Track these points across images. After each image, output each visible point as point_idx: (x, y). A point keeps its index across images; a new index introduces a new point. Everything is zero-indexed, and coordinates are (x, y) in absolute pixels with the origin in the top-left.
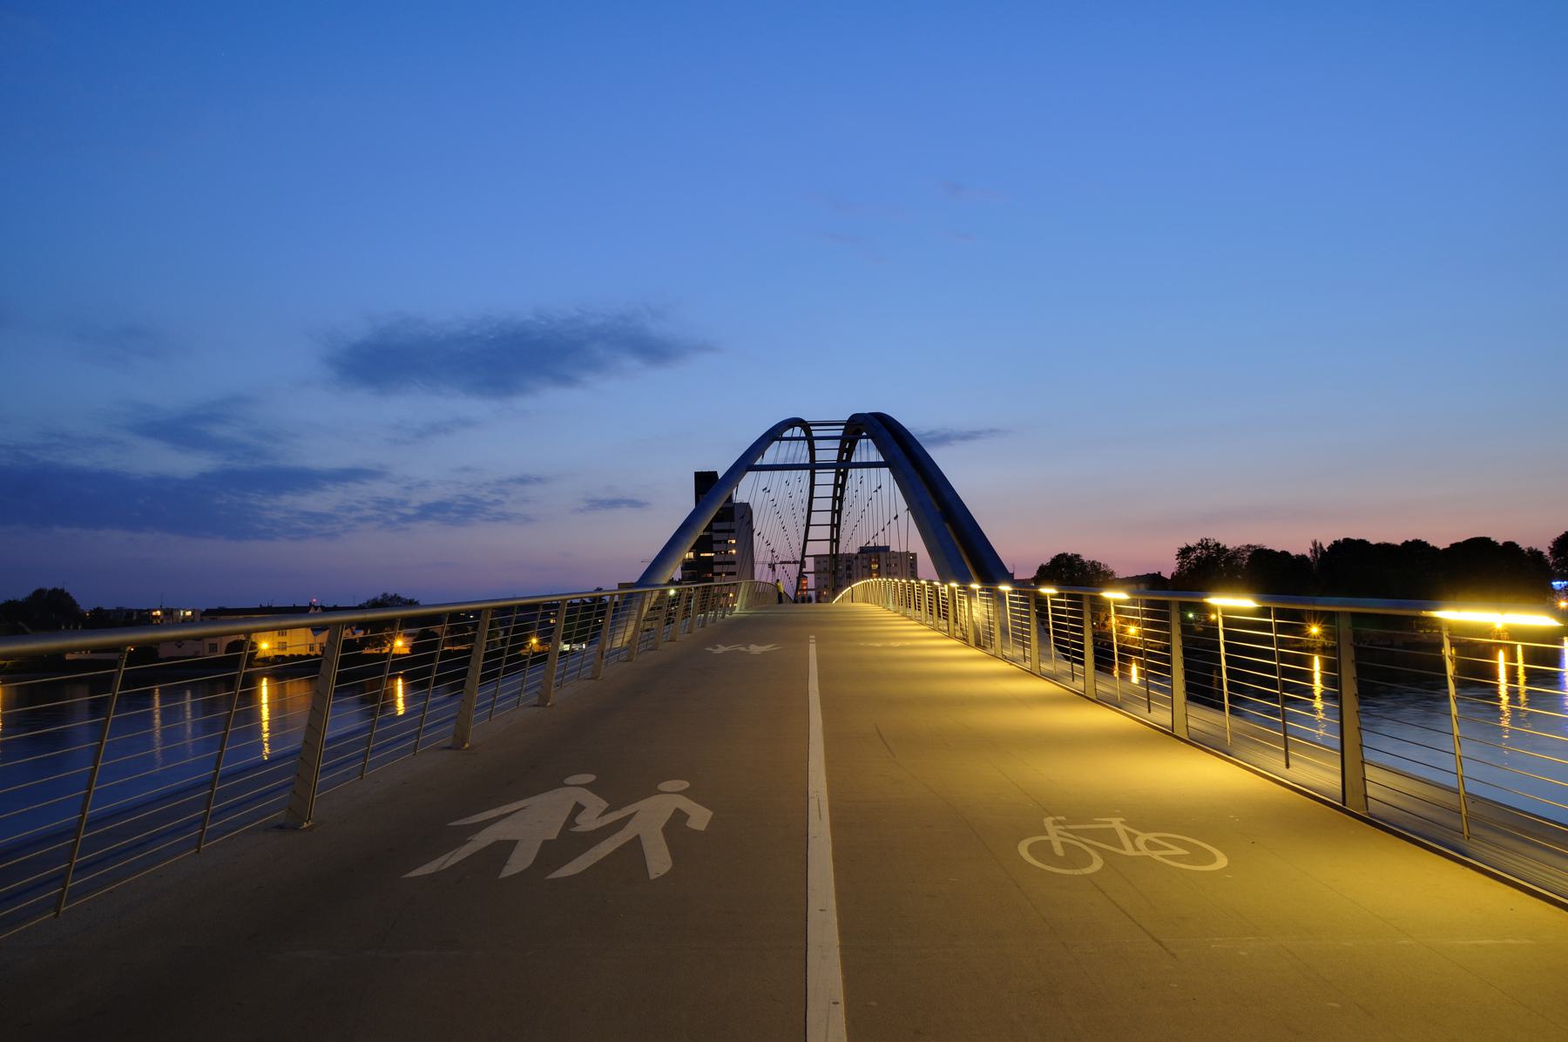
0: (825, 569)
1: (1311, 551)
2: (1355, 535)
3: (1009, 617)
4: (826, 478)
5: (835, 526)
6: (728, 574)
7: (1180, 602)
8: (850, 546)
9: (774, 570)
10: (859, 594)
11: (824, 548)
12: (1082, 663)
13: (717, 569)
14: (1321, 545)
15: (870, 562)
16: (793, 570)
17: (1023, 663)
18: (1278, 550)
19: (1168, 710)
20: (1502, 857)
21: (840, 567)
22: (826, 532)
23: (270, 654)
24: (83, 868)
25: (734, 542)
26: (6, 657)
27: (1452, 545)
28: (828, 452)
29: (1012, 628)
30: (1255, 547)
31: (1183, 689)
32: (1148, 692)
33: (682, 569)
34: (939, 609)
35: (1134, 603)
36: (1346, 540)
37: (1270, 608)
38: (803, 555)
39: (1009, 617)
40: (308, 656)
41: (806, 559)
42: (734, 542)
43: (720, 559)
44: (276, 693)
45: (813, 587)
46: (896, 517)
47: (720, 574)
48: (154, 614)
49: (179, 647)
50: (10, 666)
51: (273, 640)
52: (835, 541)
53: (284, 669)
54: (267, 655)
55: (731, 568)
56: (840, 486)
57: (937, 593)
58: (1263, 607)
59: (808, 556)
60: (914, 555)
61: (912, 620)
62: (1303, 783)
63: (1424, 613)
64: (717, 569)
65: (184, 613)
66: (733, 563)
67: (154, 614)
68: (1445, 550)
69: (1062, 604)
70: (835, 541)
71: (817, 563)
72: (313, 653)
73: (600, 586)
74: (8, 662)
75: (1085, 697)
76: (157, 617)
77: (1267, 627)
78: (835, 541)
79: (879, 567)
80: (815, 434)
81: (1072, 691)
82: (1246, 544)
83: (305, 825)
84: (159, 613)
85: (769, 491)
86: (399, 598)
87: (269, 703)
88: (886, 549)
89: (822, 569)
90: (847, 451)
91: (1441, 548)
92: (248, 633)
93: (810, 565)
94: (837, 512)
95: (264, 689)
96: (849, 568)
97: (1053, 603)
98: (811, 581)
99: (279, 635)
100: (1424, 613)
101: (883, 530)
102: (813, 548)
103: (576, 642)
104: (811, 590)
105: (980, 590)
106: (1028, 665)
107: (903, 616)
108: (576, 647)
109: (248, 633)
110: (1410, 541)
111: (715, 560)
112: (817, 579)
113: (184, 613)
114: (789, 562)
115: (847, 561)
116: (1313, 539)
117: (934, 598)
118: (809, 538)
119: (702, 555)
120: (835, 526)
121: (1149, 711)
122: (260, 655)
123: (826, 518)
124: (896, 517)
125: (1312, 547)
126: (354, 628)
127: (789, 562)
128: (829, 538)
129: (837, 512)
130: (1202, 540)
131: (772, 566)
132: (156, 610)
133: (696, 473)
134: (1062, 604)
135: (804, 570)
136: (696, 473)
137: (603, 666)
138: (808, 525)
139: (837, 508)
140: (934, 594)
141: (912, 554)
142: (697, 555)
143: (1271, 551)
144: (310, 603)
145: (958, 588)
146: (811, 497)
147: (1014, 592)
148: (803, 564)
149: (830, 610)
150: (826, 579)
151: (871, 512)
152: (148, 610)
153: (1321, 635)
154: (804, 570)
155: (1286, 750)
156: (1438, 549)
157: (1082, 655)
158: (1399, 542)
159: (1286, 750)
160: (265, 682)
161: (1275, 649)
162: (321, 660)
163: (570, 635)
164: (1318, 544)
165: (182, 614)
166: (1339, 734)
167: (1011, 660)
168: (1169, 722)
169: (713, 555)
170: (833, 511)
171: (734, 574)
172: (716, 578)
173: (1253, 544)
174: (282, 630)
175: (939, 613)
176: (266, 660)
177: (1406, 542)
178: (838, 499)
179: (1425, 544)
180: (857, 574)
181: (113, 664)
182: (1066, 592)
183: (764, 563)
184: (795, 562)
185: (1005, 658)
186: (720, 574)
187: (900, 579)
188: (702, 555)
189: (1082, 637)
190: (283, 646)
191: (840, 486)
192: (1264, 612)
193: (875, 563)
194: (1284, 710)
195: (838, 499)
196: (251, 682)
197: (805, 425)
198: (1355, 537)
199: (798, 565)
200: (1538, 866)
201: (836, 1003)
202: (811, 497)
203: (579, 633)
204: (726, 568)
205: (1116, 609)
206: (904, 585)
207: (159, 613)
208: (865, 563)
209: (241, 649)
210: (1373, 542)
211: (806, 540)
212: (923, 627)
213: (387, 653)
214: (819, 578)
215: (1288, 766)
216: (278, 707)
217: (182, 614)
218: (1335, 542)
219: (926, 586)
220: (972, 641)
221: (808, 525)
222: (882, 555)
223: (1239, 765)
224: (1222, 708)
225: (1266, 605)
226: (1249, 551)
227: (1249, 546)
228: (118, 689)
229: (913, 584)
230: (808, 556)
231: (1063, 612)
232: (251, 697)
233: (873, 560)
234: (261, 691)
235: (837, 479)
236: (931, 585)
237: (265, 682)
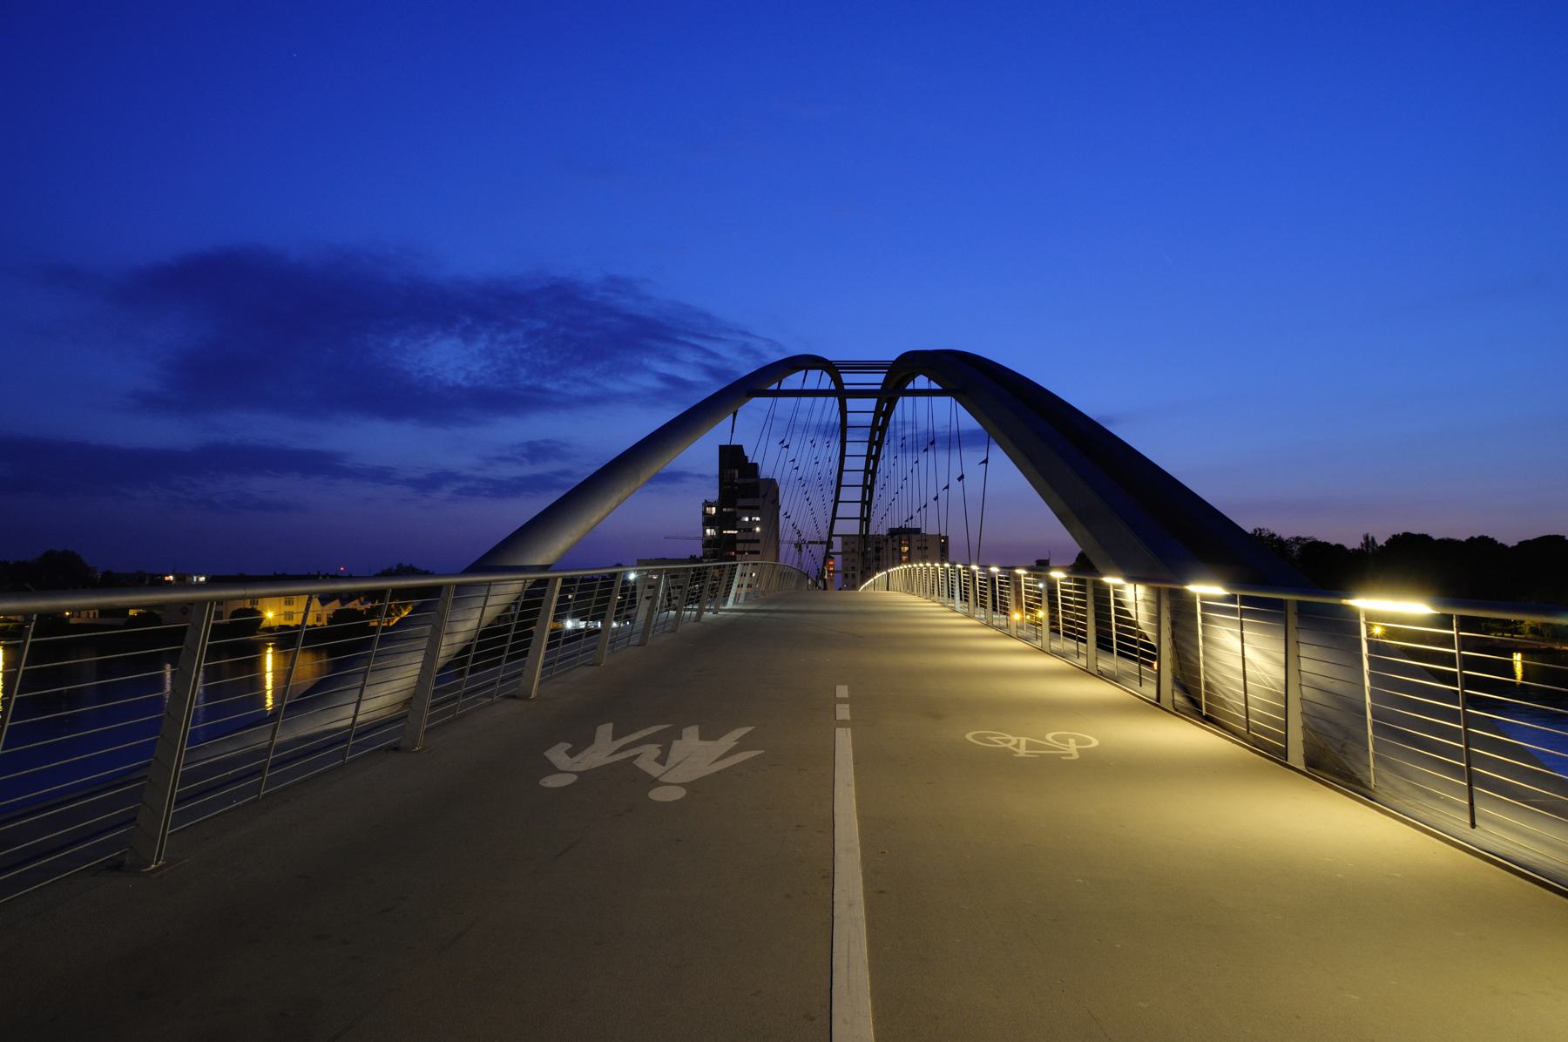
0: (853, 551)
1: (1362, 545)
2: (1416, 530)
3: (1367, 682)
4: (858, 448)
5: (866, 503)
6: (751, 552)
7: (1298, 601)
8: (879, 527)
9: (800, 550)
10: (897, 582)
11: (853, 528)
12: (986, 607)
13: (739, 547)
14: (1373, 539)
15: (901, 545)
16: (819, 550)
17: (1076, 660)
18: (1333, 543)
19: (1456, 806)
20: (1442, 817)
21: (869, 549)
22: (855, 510)
23: (275, 624)
24: (466, 694)
25: (758, 519)
26: (5, 613)
27: (1520, 543)
28: (862, 411)
29: (1117, 636)
30: (1305, 539)
31: (1094, 639)
32: (1140, 668)
33: (704, 546)
34: (960, 587)
35: (1232, 599)
36: (1406, 535)
37: (1236, 596)
38: (831, 534)
39: (1367, 682)
40: (315, 626)
41: (833, 539)
42: (758, 519)
43: (743, 536)
44: (282, 662)
45: (840, 569)
46: (925, 506)
47: (742, 553)
48: (167, 578)
49: (185, 613)
50: (12, 628)
51: (280, 608)
52: (865, 520)
53: (286, 639)
54: (273, 624)
55: (754, 547)
56: (873, 458)
57: (974, 579)
58: (1442, 614)
59: (835, 536)
60: (946, 538)
61: (945, 606)
62: (1493, 851)
63: (1345, 602)
64: (739, 547)
65: (197, 579)
66: (757, 541)
67: (167, 578)
68: (1513, 547)
69: (1070, 587)
70: (865, 520)
71: (845, 544)
72: (319, 624)
73: (620, 562)
74: (11, 625)
75: (1086, 672)
76: (169, 581)
77: (1448, 641)
78: (865, 519)
79: (909, 551)
80: (833, 402)
81: (1131, 693)
82: (1295, 536)
83: (417, 749)
84: (171, 578)
85: (787, 447)
86: (414, 568)
87: (274, 671)
88: (917, 531)
89: (850, 550)
90: (873, 457)
91: (1510, 546)
92: (254, 599)
93: (837, 545)
94: (868, 488)
95: (269, 659)
96: (878, 550)
97: (1062, 586)
98: (837, 563)
99: (286, 602)
100: (1345, 602)
101: (936, 498)
102: (842, 528)
103: (594, 619)
104: (837, 572)
105: (979, 571)
106: (1039, 644)
107: (987, 625)
108: (592, 625)
109: (254, 599)
110: (1476, 536)
111: (738, 538)
112: (844, 560)
113: (197, 579)
114: (816, 543)
115: (876, 542)
116: (1365, 533)
117: (936, 577)
118: (837, 516)
119: (725, 532)
120: (866, 503)
121: (1141, 685)
122: (265, 624)
123: (857, 494)
124: (925, 506)
125: (1363, 542)
126: (362, 599)
127: (816, 543)
128: (860, 500)
129: (868, 488)
130: (1255, 531)
131: (799, 546)
132: (168, 576)
133: (720, 446)
134: (1070, 587)
135: (831, 551)
136: (720, 446)
137: (650, 635)
138: (839, 486)
139: (871, 468)
140: (971, 580)
141: (943, 538)
142: (720, 533)
143: (1327, 544)
144: (319, 572)
145: (999, 573)
146: (841, 470)
147: (1029, 575)
148: (829, 544)
149: (862, 608)
150: (853, 560)
151: (904, 494)
152: (161, 575)
153: (1384, 635)
154: (831, 551)
155: (1471, 804)
156: (1507, 547)
157: (1085, 634)
158: (1464, 539)
159: (1471, 804)
160: (270, 650)
161: (1457, 670)
162: (181, 649)
163: (587, 612)
164: (1370, 539)
165: (195, 580)
166: (1284, 703)
167: (1061, 655)
168: (1085, 664)
169: (736, 532)
170: (865, 486)
171: (758, 552)
172: (738, 556)
173: (1303, 536)
174: (289, 598)
175: (994, 601)
176: (270, 629)
177: (1472, 538)
178: (870, 472)
179: (1492, 542)
180: (887, 557)
181: (596, 580)
182: (1239, 593)
183: (790, 543)
184: (821, 543)
185: (1053, 653)
186: (743, 553)
187: (933, 563)
188: (725, 532)
189: (1086, 618)
190: (289, 615)
191: (873, 458)
192: (1445, 621)
193: (905, 545)
194: (1468, 752)
195: (870, 472)
196: (257, 649)
197: (832, 368)
198: (1416, 531)
199: (825, 546)
200: (1495, 839)
201: (848, 785)
202: (841, 470)
203: (595, 610)
204: (747, 547)
205: (1203, 605)
206: (921, 569)
207: (171, 578)
208: (896, 546)
209: (248, 621)
210: (1436, 537)
211: (834, 518)
212: (936, 604)
213: (375, 627)
214: (847, 560)
215: (1473, 825)
216: (284, 677)
217: (195, 580)
218: (1394, 536)
219: (950, 570)
220: (1296, 756)
221: (837, 501)
222: (914, 537)
223: (1125, 690)
224: (1112, 651)
225: (1234, 593)
226: (1298, 544)
227: (1298, 539)
228: (23, 663)
229: (959, 570)
230: (835, 536)
231: (1070, 594)
232: (256, 665)
233: (903, 542)
234: (265, 661)
235: (870, 449)
236: (968, 569)
237: (270, 650)
